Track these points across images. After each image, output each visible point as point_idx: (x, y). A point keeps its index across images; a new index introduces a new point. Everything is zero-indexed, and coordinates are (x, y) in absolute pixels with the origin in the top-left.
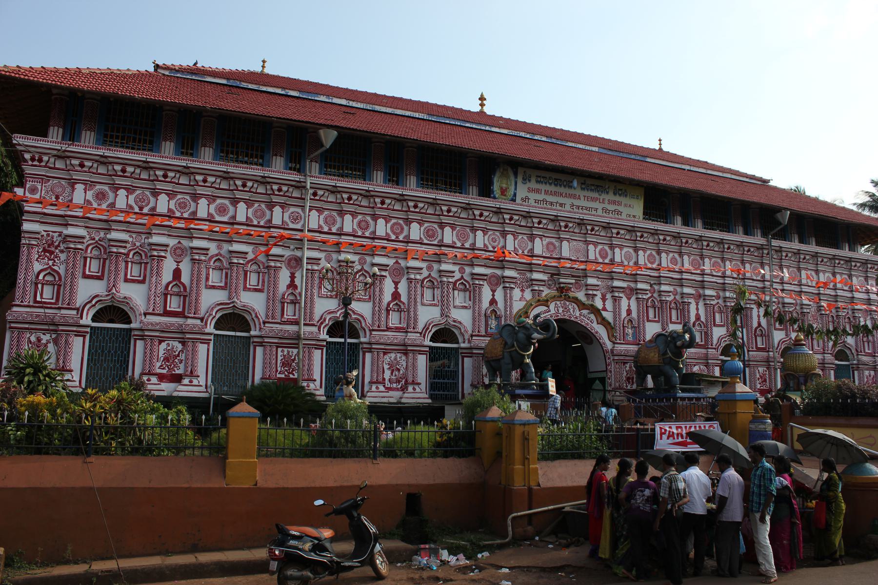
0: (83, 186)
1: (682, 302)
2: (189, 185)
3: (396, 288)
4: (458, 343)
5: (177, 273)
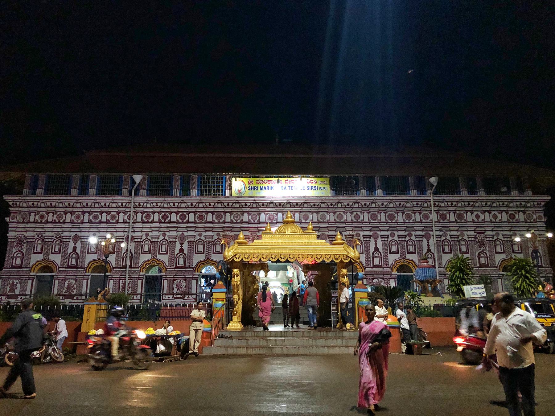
0: (34, 214)
1: (468, 240)
2: (222, 208)
3: (182, 247)
4: (412, 272)
5: (75, 249)
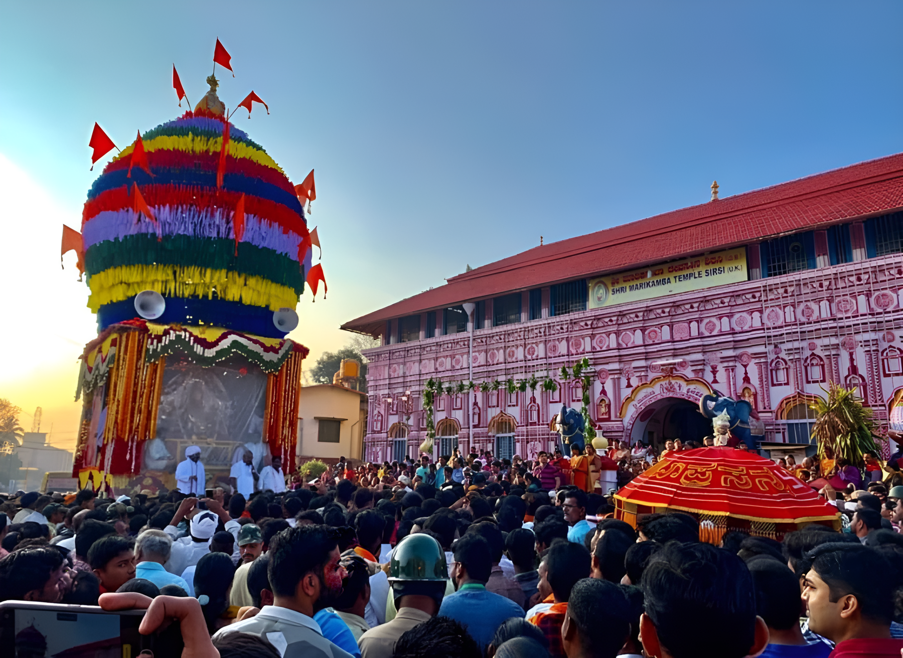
5: (603, 392)
